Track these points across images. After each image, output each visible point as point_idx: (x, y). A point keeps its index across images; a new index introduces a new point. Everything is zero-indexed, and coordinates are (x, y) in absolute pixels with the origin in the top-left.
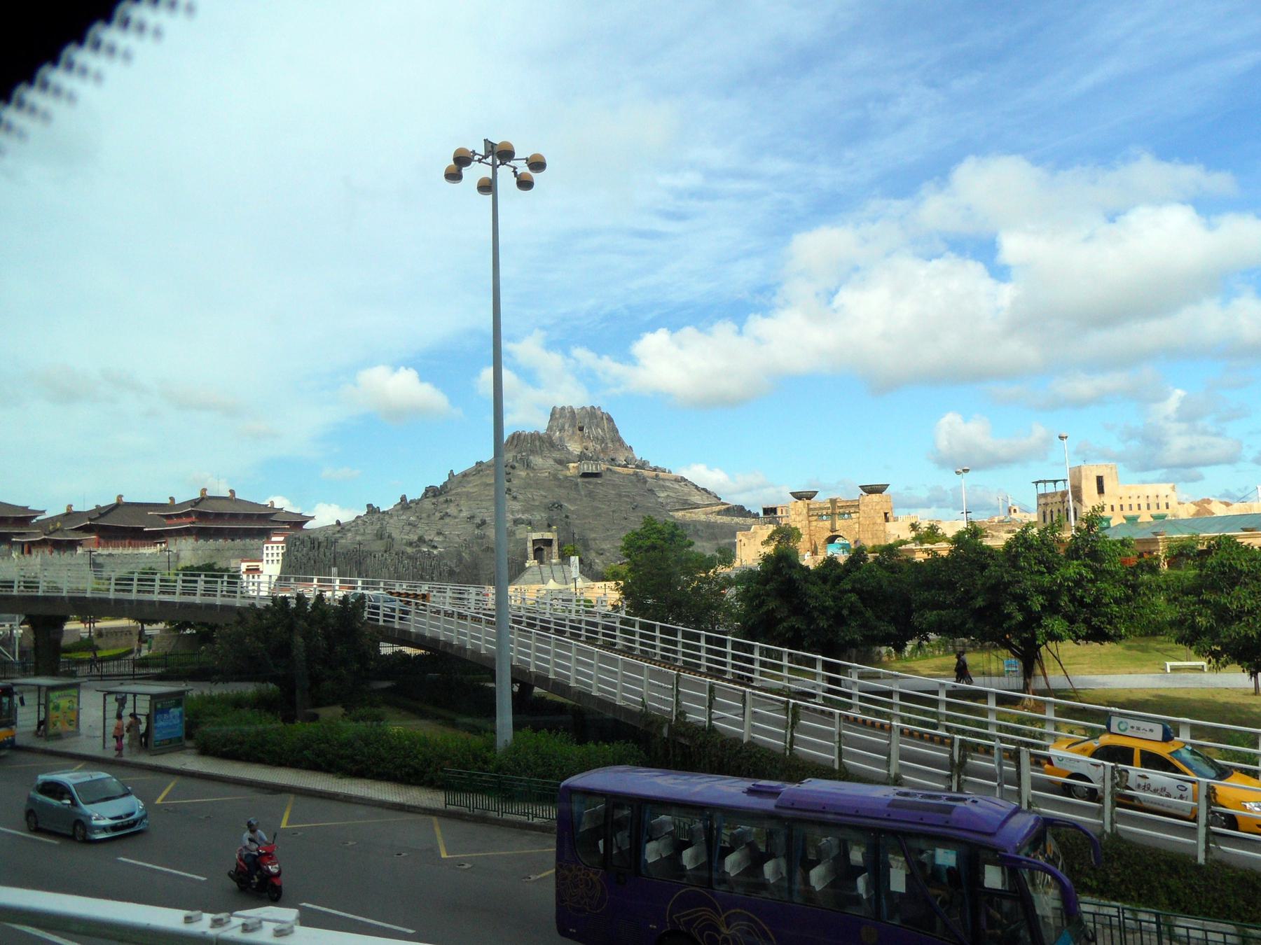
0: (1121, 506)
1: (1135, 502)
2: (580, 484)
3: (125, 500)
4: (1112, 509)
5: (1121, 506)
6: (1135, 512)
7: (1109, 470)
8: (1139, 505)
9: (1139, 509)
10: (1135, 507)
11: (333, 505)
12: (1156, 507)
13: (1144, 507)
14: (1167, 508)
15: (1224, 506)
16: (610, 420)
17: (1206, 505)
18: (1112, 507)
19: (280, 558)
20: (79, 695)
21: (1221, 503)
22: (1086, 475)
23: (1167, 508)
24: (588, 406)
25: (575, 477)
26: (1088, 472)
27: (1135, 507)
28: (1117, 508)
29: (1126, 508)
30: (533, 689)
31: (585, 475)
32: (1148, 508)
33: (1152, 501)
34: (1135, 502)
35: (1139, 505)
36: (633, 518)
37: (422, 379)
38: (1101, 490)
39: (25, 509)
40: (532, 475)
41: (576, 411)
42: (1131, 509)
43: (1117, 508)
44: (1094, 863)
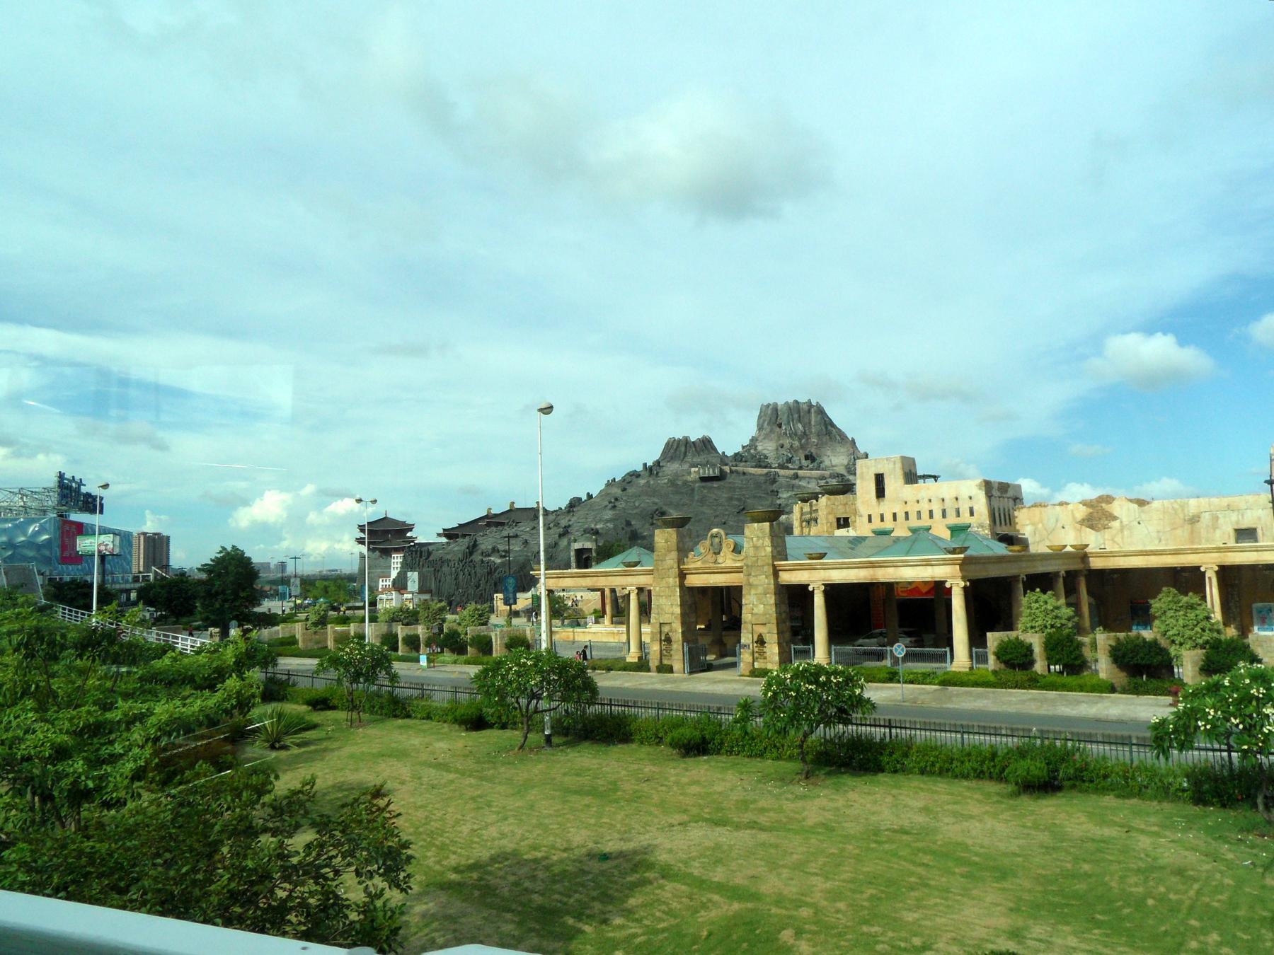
0: (907, 513)
1: (925, 507)
2: (696, 489)
3: (516, 506)
4: (931, 516)
5: (907, 513)
6: (925, 521)
7: (891, 466)
8: (931, 512)
9: (895, 519)
10: (925, 515)
11: (1086, 485)
12: (954, 513)
13: (937, 514)
14: (972, 514)
15: (1136, 506)
16: (821, 411)
17: (1103, 505)
18: (895, 515)
19: (399, 566)
20: (661, 659)
21: (1131, 501)
22: (862, 473)
23: (972, 514)
24: (791, 400)
25: (694, 482)
26: (865, 470)
27: (925, 515)
28: (901, 516)
29: (913, 516)
30: (1103, 680)
31: (703, 479)
32: (944, 516)
33: (949, 506)
34: (925, 507)
35: (931, 512)
36: (731, 523)
37: (1182, 342)
38: (880, 493)
39: (404, 523)
40: (652, 482)
41: (779, 408)
42: (882, 520)
43: (901, 516)
44: (1249, 937)
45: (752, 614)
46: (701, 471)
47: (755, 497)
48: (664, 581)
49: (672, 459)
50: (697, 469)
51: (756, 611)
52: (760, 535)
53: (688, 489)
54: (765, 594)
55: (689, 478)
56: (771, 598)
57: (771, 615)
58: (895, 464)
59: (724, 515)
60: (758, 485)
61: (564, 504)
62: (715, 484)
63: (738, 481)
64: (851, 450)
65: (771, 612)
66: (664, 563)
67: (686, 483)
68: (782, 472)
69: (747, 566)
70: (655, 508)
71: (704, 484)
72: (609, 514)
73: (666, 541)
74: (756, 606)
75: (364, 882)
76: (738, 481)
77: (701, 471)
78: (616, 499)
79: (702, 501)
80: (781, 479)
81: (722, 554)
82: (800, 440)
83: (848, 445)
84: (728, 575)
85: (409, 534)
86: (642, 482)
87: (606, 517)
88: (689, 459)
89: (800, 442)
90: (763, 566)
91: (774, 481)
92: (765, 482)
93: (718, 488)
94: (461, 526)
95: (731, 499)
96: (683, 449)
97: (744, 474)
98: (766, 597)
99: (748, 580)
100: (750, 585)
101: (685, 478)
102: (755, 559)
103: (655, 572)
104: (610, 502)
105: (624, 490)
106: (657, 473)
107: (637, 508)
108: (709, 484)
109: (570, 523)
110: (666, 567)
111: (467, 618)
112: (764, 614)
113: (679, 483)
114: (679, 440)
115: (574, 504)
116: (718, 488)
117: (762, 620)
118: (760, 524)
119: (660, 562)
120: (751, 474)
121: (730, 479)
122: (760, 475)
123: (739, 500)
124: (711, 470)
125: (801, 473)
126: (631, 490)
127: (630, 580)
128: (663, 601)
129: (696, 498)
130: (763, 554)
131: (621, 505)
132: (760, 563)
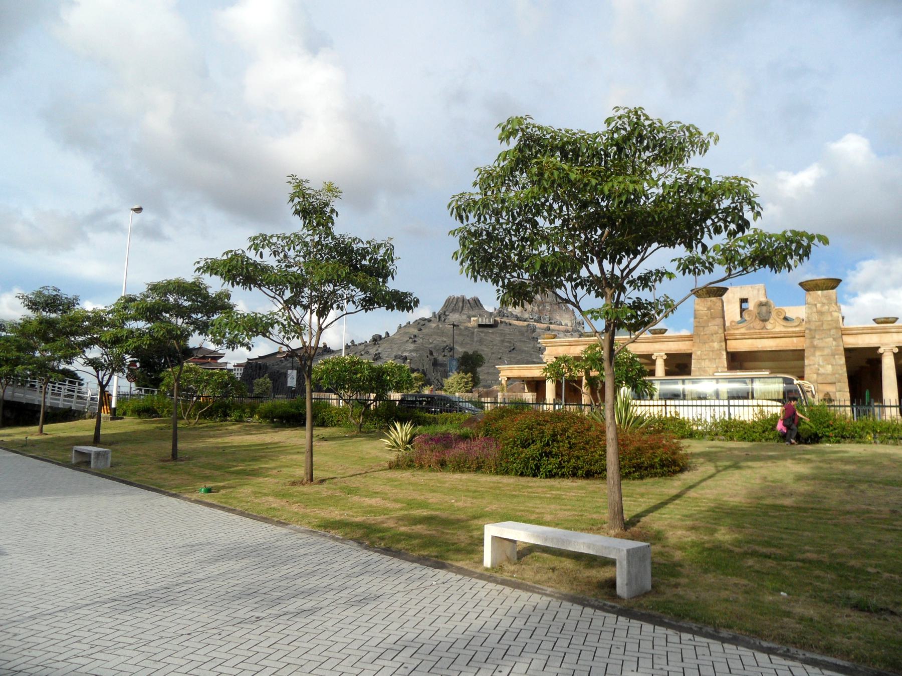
2: (475, 333)
31: (480, 326)
40: (441, 326)
45: (818, 374)
46: (480, 320)
47: (521, 341)
48: (707, 346)
49: (453, 311)
50: (475, 319)
51: (822, 371)
52: (825, 301)
53: (470, 332)
54: (833, 355)
55: (469, 325)
56: (840, 358)
57: (841, 375)
58: (758, 291)
59: (499, 352)
60: (522, 333)
61: (368, 338)
62: (490, 330)
63: (507, 330)
64: (573, 317)
65: (840, 372)
66: (706, 329)
67: (467, 328)
68: (538, 325)
69: (810, 330)
70: (445, 345)
71: (481, 329)
72: (411, 346)
73: (709, 309)
74: (823, 367)
75: (737, 594)
76: (507, 330)
77: (480, 320)
78: (415, 336)
79: (481, 342)
80: (538, 330)
81: (771, 321)
82: (538, 307)
83: (571, 313)
84: (778, 340)
85: (220, 361)
86: (433, 325)
87: (409, 348)
88: (465, 311)
89: (538, 307)
90: (830, 330)
91: (534, 331)
92: (527, 332)
93: (492, 333)
94: (260, 358)
95: (503, 341)
96: (461, 304)
97: (510, 324)
98: (834, 358)
99: (812, 342)
100: (815, 348)
101: (466, 324)
102: (820, 323)
103: (696, 339)
104: (410, 338)
105: (420, 330)
106: (445, 320)
107: (431, 343)
108: (485, 330)
109: (379, 351)
110: (708, 332)
111: (455, 385)
112: (833, 374)
113: (462, 328)
114: (458, 298)
115: (377, 339)
116: (492, 333)
117: (831, 379)
118: (825, 292)
119: (702, 329)
120: (515, 325)
121: (501, 327)
122: (522, 326)
123: (510, 342)
124: (487, 320)
125: (552, 326)
126: (425, 331)
127: (657, 346)
128: (705, 364)
129: (475, 339)
130: (830, 319)
131: (419, 341)
132: (825, 327)
